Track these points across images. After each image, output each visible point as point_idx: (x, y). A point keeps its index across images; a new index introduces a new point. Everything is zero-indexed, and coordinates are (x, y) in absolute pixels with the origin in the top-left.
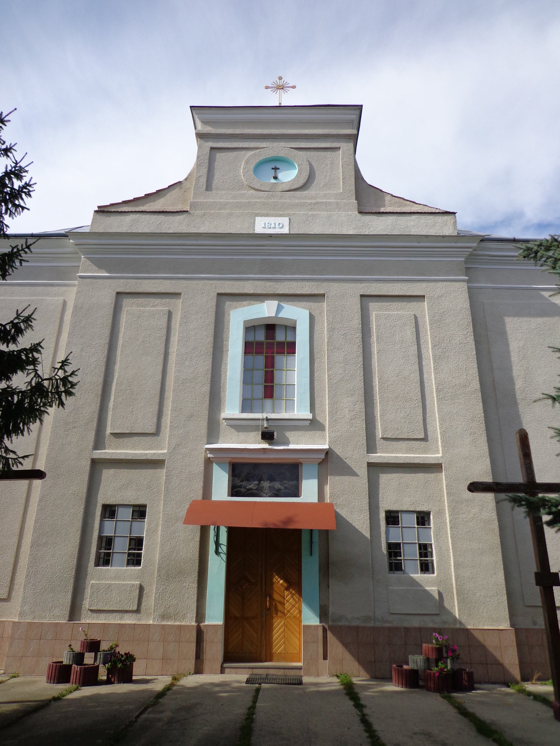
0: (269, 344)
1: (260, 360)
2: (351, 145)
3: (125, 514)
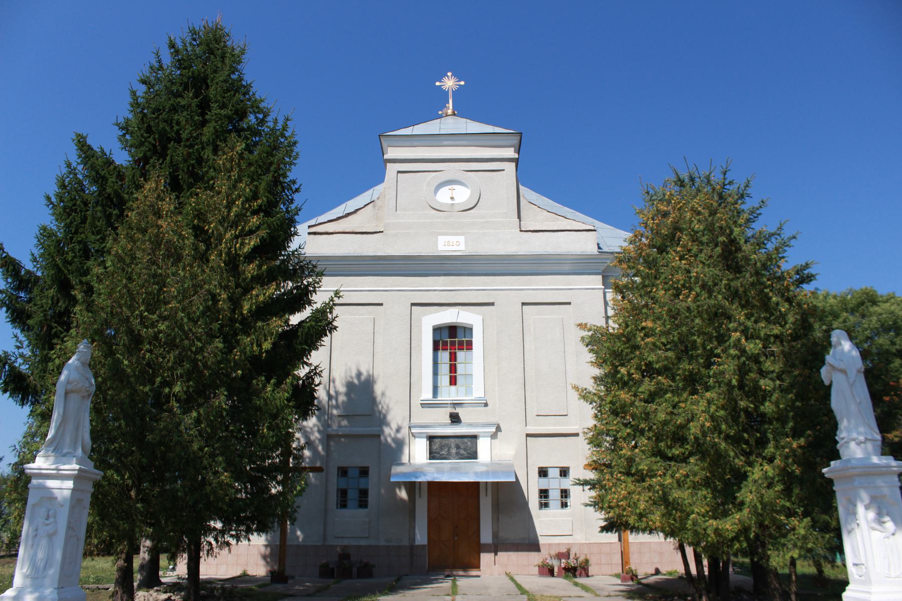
0: (451, 339)
2: (514, 164)
3: (554, 473)
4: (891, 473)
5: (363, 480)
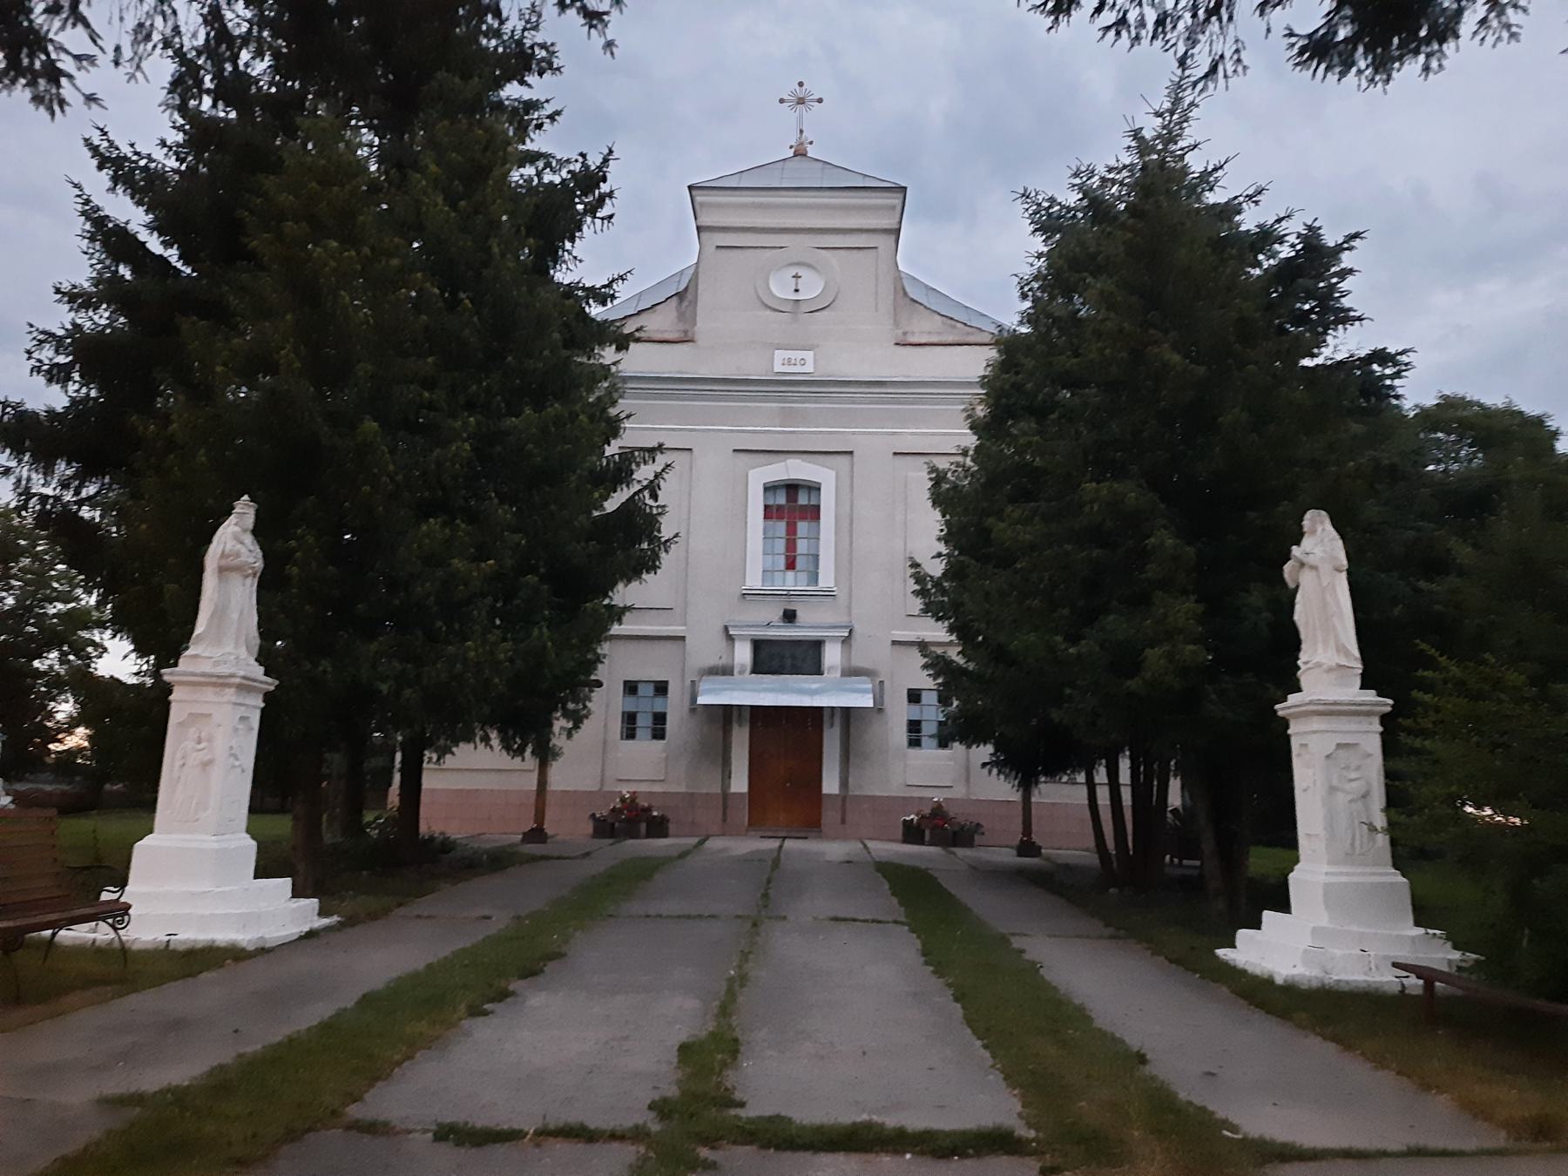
1: (781, 527)
2: (893, 237)
4: (1368, 714)
5: (659, 701)
